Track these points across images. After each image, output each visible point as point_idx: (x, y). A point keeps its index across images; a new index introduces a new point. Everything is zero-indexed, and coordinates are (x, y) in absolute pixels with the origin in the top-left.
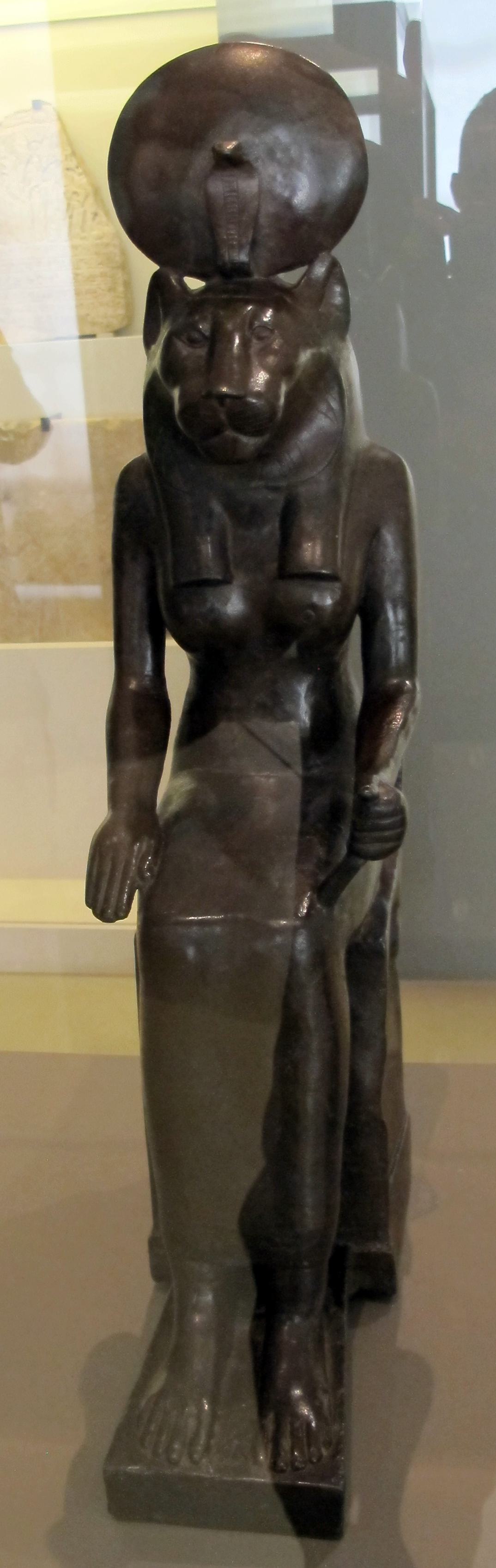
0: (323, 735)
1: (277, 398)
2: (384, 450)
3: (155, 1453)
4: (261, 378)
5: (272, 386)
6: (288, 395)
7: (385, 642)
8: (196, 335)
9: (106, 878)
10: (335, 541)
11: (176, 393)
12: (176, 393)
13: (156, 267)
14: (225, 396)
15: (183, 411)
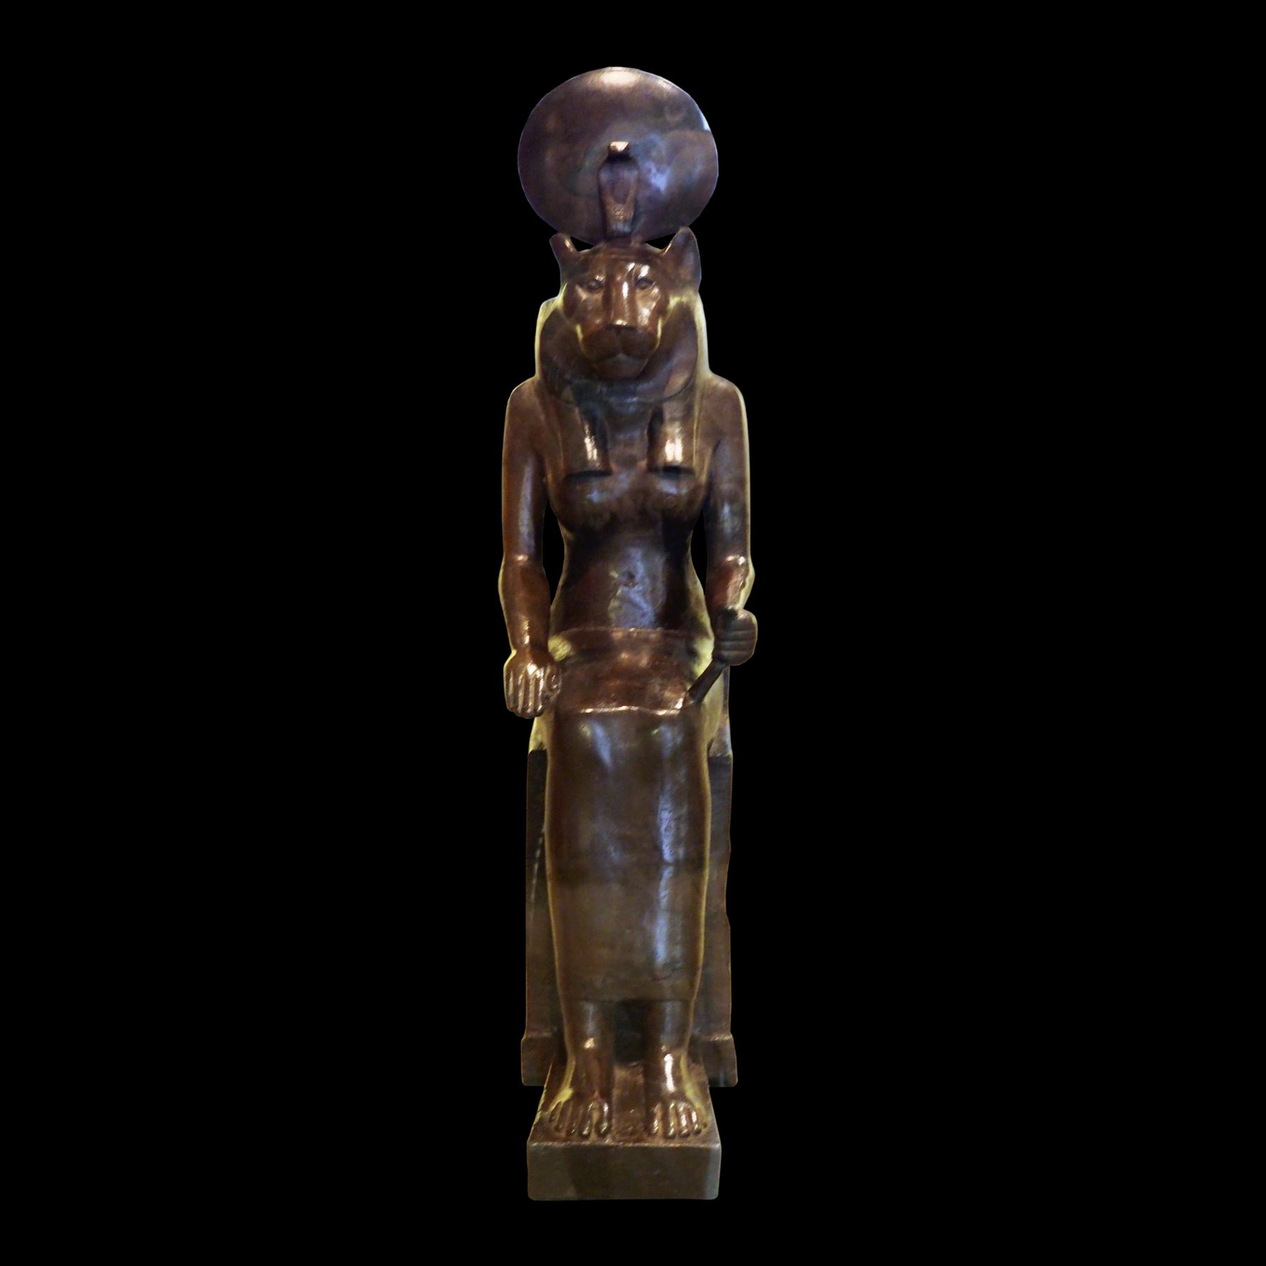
0: (628, 353)
3: (569, 1133)
9: (521, 694)
11: (578, 329)
12: (578, 329)
15: (585, 339)
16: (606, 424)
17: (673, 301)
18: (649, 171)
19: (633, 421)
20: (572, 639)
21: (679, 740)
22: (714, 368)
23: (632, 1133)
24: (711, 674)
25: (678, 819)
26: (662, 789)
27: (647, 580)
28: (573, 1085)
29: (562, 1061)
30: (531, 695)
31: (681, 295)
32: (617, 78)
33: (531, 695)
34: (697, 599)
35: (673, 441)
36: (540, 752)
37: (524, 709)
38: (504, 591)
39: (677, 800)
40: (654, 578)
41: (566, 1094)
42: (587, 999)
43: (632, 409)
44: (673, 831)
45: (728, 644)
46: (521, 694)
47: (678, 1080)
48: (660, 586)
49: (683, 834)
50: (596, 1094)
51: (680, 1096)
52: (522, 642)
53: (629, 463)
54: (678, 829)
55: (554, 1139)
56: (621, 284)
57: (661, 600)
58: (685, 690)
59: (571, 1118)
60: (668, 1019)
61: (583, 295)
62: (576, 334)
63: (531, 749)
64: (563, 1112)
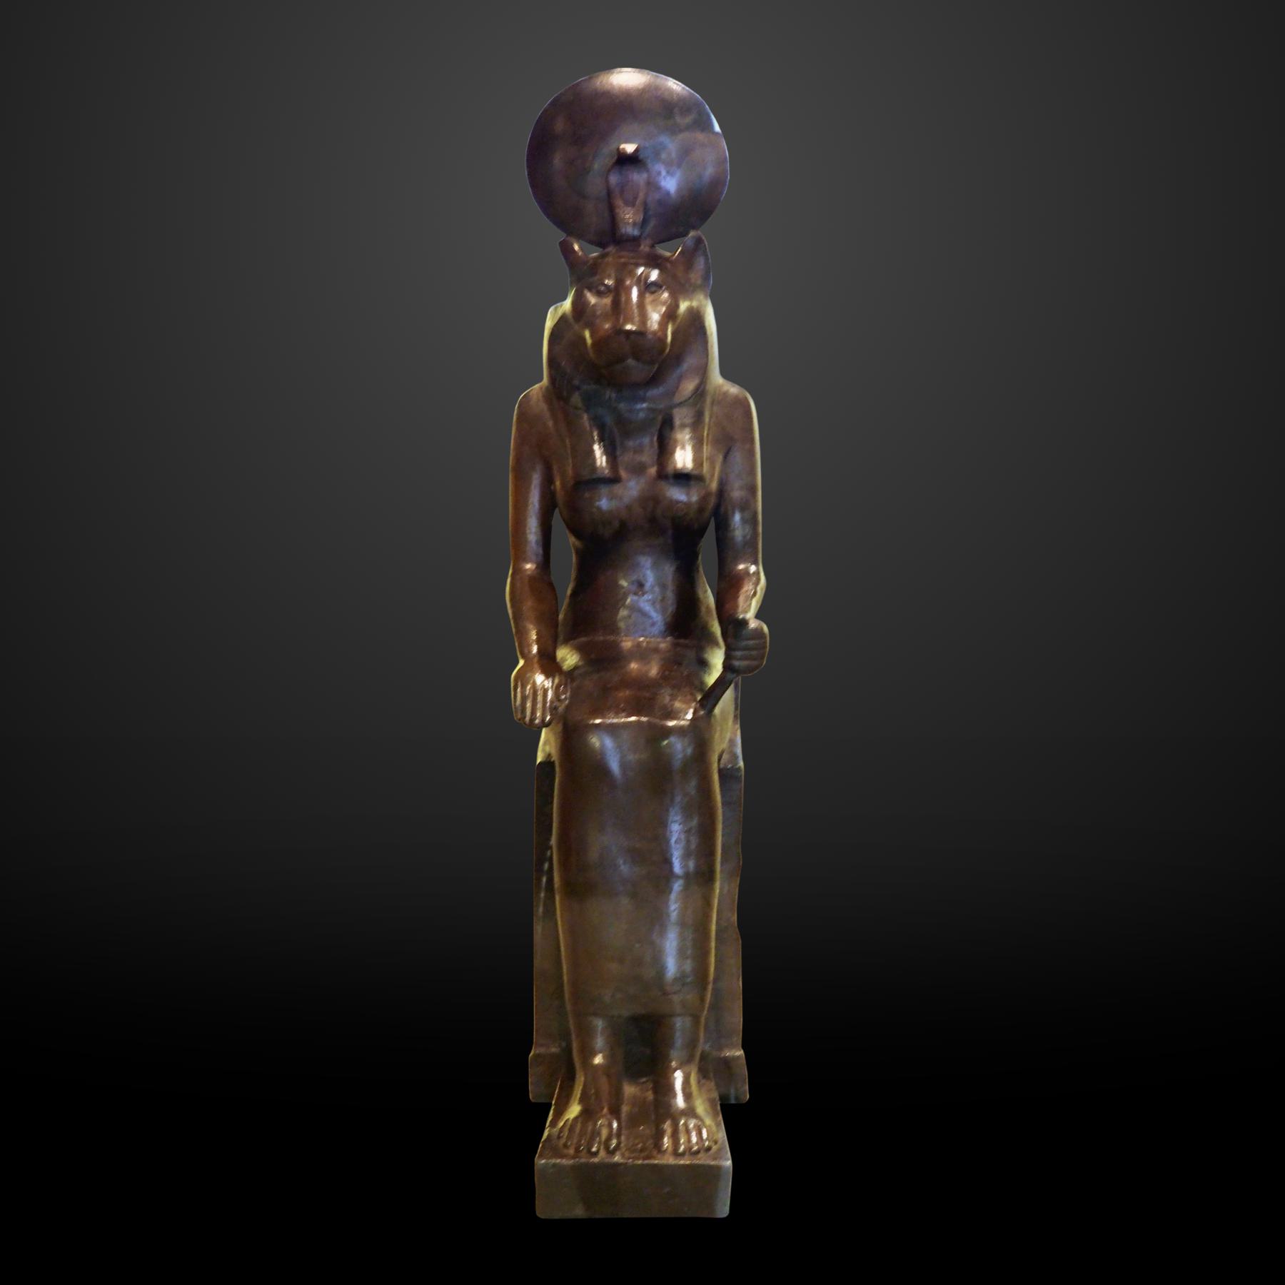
0: (637, 358)
1: (666, 336)
3: (577, 1150)
4: (655, 317)
5: (663, 324)
6: (673, 334)
8: (603, 288)
9: (529, 705)
10: (565, 864)
11: (587, 334)
12: (587, 334)
13: (562, 236)
14: (629, 332)
15: (594, 344)
17: (683, 306)
18: (659, 173)
19: (643, 427)
20: (580, 649)
21: (689, 751)
22: (724, 374)
23: (642, 1150)
24: (721, 684)
25: (688, 832)
26: (672, 800)
27: (657, 589)
28: (581, 1101)
29: (571, 1077)
30: (539, 706)
31: (691, 300)
32: (627, 79)
33: (539, 706)
34: (708, 608)
35: (683, 448)
36: (548, 764)
37: (532, 720)
38: (511, 600)
39: (687, 812)
40: (663, 587)
41: (574, 1110)
42: (595, 1014)
43: (642, 415)
44: (683, 844)
45: (739, 653)
46: (529, 705)
47: (688, 1096)
48: (670, 595)
49: (693, 846)
50: (605, 1110)
51: (690, 1112)
52: (530, 652)
53: (639, 470)
54: (688, 841)
55: (562, 1157)
56: (630, 288)
57: (671, 609)
58: (695, 700)
59: (580, 1134)
60: (678, 1034)
61: (592, 299)
62: (584, 339)
63: (539, 760)
64: (572, 1129)
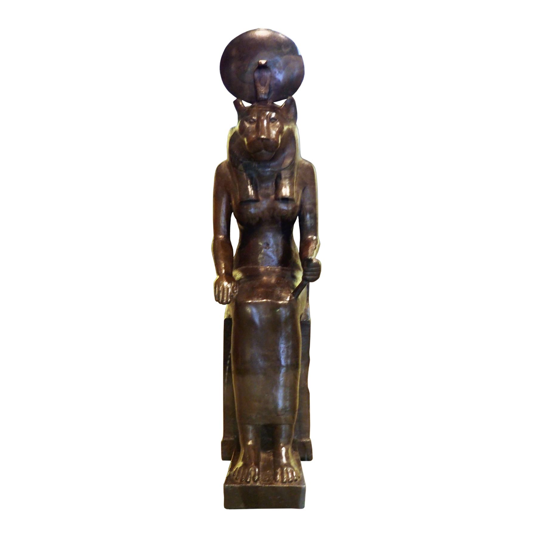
0: (266, 150)
1: (278, 140)
2: (307, 161)
3: (241, 481)
4: (274, 133)
5: (277, 135)
6: (281, 139)
7: (219, 223)
8: (252, 120)
9: (221, 294)
11: (245, 140)
12: (245, 140)
13: (235, 98)
14: (263, 139)
15: (248, 144)
16: (257, 180)
17: (286, 128)
18: (275, 72)
19: (269, 179)
20: (242, 271)
21: (288, 314)
23: (268, 481)
25: (287, 348)
26: (281, 334)
27: (274, 246)
28: (243, 460)
29: (239, 450)
30: (225, 295)
31: (289, 125)
33: (225, 295)
34: (296, 254)
35: (286, 187)
39: (287, 339)
40: (277, 245)
42: (249, 424)
43: (268, 173)
44: (285, 353)
45: (309, 273)
46: (221, 294)
47: (287, 458)
48: (280, 249)
49: (290, 354)
50: (253, 464)
52: (221, 272)
53: (267, 196)
54: (288, 352)
55: (235, 483)
56: (263, 121)
57: (280, 254)
58: (290, 292)
60: (283, 432)
61: (247, 125)
62: (244, 142)
64: (239, 472)
